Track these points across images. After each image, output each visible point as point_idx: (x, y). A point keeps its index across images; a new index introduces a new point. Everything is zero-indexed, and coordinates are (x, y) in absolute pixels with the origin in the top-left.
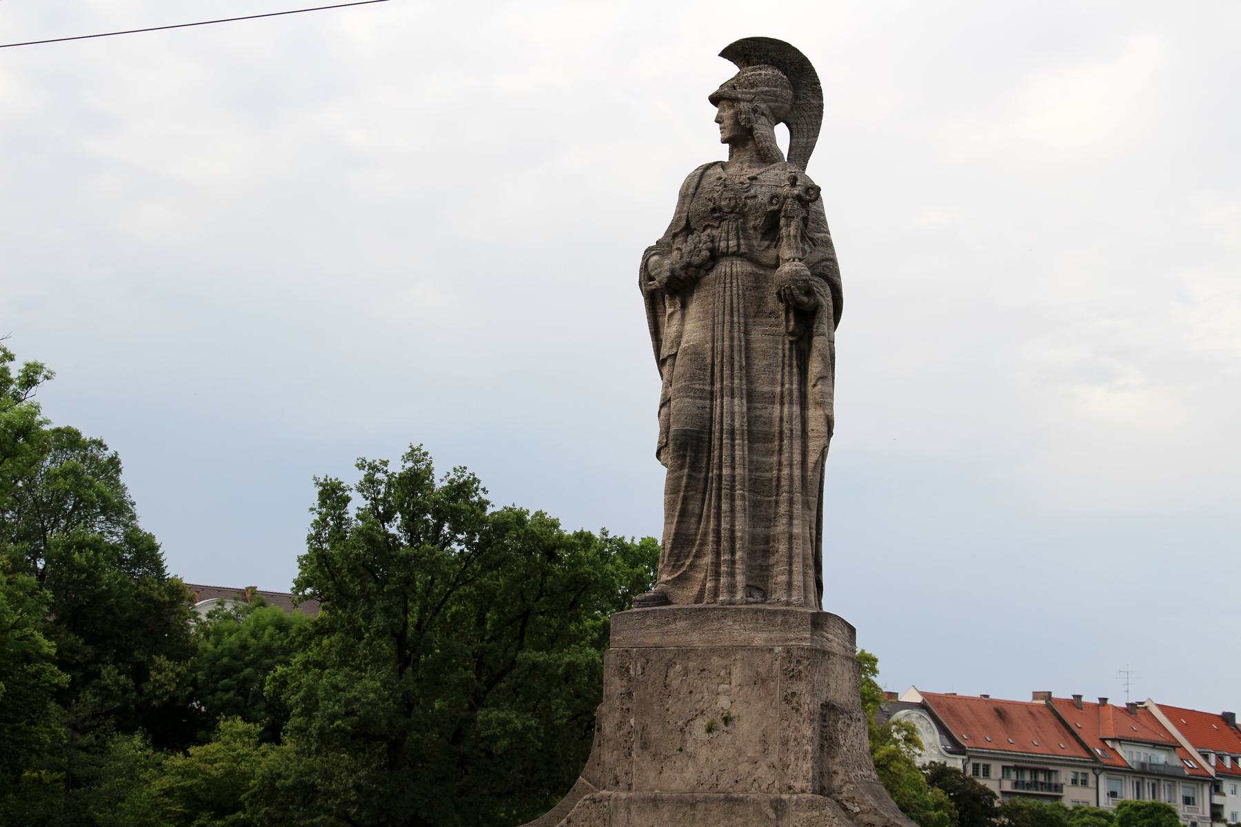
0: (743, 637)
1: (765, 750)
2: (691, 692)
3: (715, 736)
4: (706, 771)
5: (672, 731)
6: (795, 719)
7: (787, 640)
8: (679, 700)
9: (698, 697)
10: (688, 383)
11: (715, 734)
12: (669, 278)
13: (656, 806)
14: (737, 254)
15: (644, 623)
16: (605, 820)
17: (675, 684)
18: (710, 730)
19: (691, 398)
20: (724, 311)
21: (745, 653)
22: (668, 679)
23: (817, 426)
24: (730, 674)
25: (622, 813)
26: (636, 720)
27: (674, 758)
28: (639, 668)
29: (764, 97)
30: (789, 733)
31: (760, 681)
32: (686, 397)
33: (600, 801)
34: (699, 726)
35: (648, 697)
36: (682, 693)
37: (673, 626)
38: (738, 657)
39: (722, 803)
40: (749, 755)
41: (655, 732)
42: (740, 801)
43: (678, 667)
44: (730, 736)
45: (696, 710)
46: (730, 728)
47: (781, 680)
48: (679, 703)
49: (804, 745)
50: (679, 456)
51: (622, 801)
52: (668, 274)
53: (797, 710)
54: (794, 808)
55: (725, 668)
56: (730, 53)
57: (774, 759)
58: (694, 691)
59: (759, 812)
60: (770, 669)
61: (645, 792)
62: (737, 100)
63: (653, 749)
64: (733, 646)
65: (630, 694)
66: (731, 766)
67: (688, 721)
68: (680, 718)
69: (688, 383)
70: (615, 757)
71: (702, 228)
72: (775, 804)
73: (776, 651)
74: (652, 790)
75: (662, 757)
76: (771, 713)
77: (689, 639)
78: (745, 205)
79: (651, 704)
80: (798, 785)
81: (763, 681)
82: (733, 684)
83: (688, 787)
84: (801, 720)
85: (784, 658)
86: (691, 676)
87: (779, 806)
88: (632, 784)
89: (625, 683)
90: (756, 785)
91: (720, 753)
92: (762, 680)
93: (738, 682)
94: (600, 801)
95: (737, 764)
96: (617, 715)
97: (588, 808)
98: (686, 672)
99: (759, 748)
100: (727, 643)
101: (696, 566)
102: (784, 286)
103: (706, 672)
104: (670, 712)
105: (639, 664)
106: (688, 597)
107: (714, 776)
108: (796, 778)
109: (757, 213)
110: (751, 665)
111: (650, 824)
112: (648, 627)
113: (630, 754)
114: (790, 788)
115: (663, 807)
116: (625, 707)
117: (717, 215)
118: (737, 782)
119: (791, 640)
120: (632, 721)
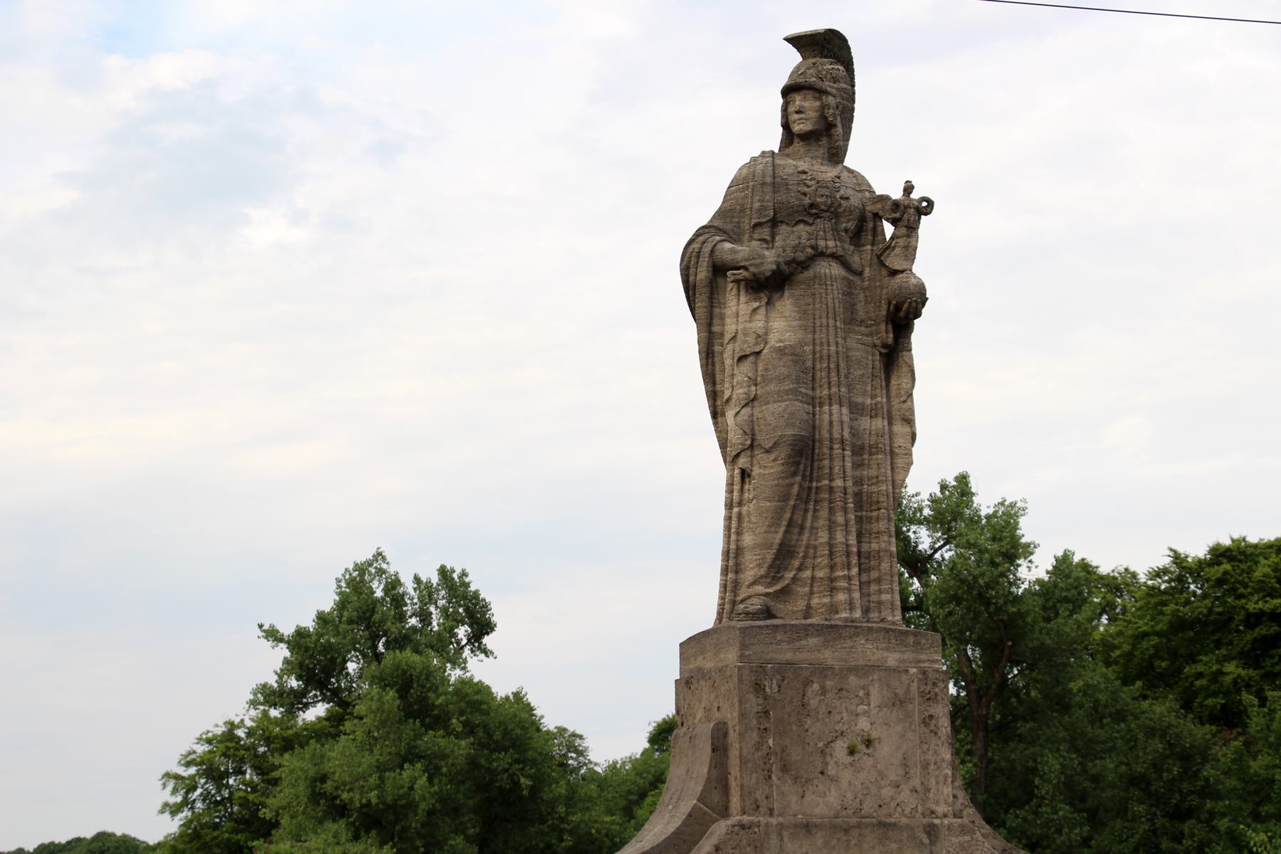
0: (876, 657)
1: (907, 773)
2: (830, 712)
3: (856, 759)
4: (849, 795)
5: (812, 753)
6: (934, 742)
7: (919, 661)
8: (819, 720)
9: (837, 718)
10: (795, 386)
11: (856, 757)
12: (774, 272)
13: (809, 832)
14: (834, 256)
15: (774, 638)
16: (756, 847)
17: (813, 703)
18: (852, 752)
19: (801, 402)
20: (827, 315)
21: (883, 674)
22: (806, 698)
23: (905, 443)
24: (868, 694)
25: (774, 840)
26: (774, 740)
27: (816, 782)
28: (774, 685)
29: (843, 94)
30: (929, 756)
31: (898, 703)
32: (797, 400)
33: (750, 828)
34: (840, 747)
35: (786, 716)
36: (821, 713)
37: (804, 642)
38: (876, 677)
39: (875, 828)
40: (891, 778)
41: (795, 754)
42: (894, 826)
43: (816, 686)
44: (871, 759)
45: (836, 731)
46: (870, 751)
47: (919, 702)
48: (818, 724)
49: (944, 769)
50: (794, 462)
51: (774, 827)
52: (774, 267)
53: (936, 733)
54: (947, 833)
55: (863, 688)
56: (795, 41)
57: (916, 782)
58: (834, 712)
59: (913, 837)
60: (908, 691)
61: (788, 817)
62: (826, 93)
63: (793, 772)
64: (867, 666)
65: (766, 713)
66: (873, 789)
67: (829, 743)
68: (820, 739)
69: (795, 386)
70: (754, 780)
71: (794, 222)
72: (928, 829)
73: (911, 673)
74: (795, 815)
75: (803, 780)
76: (910, 735)
77: (822, 657)
78: (840, 205)
79: (790, 724)
80: (941, 809)
81: (901, 702)
82: (872, 707)
83: (832, 812)
84: (940, 743)
85: (920, 680)
86: (829, 695)
87: (931, 831)
88: (773, 809)
89: (761, 701)
90: (899, 809)
91: (862, 776)
92: (901, 701)
93: (877, 704)
94: (750, 828)
95: (880, 788)
96: (755, 735)
97: (738, 834)
98: (824, 691)
99: (901, 771)
100: (861, 663)
101: (798, 580)
102: (911, 298)
103: (844, 692)
104: (810, 733)
105: (774, 682)
106: (794, 612)
107: (858, 800)
108: (937, 803)
109: (850, 215)
110: (888, 686)
111: (804, 851)
112: (779, 643)
113: (770, 777)
114: (932, 812)
115: (816, 833)
116: (762, 727)
117: (814, 211)
118: (880, 806)
119: (924, 662)
120: (771, 742)
